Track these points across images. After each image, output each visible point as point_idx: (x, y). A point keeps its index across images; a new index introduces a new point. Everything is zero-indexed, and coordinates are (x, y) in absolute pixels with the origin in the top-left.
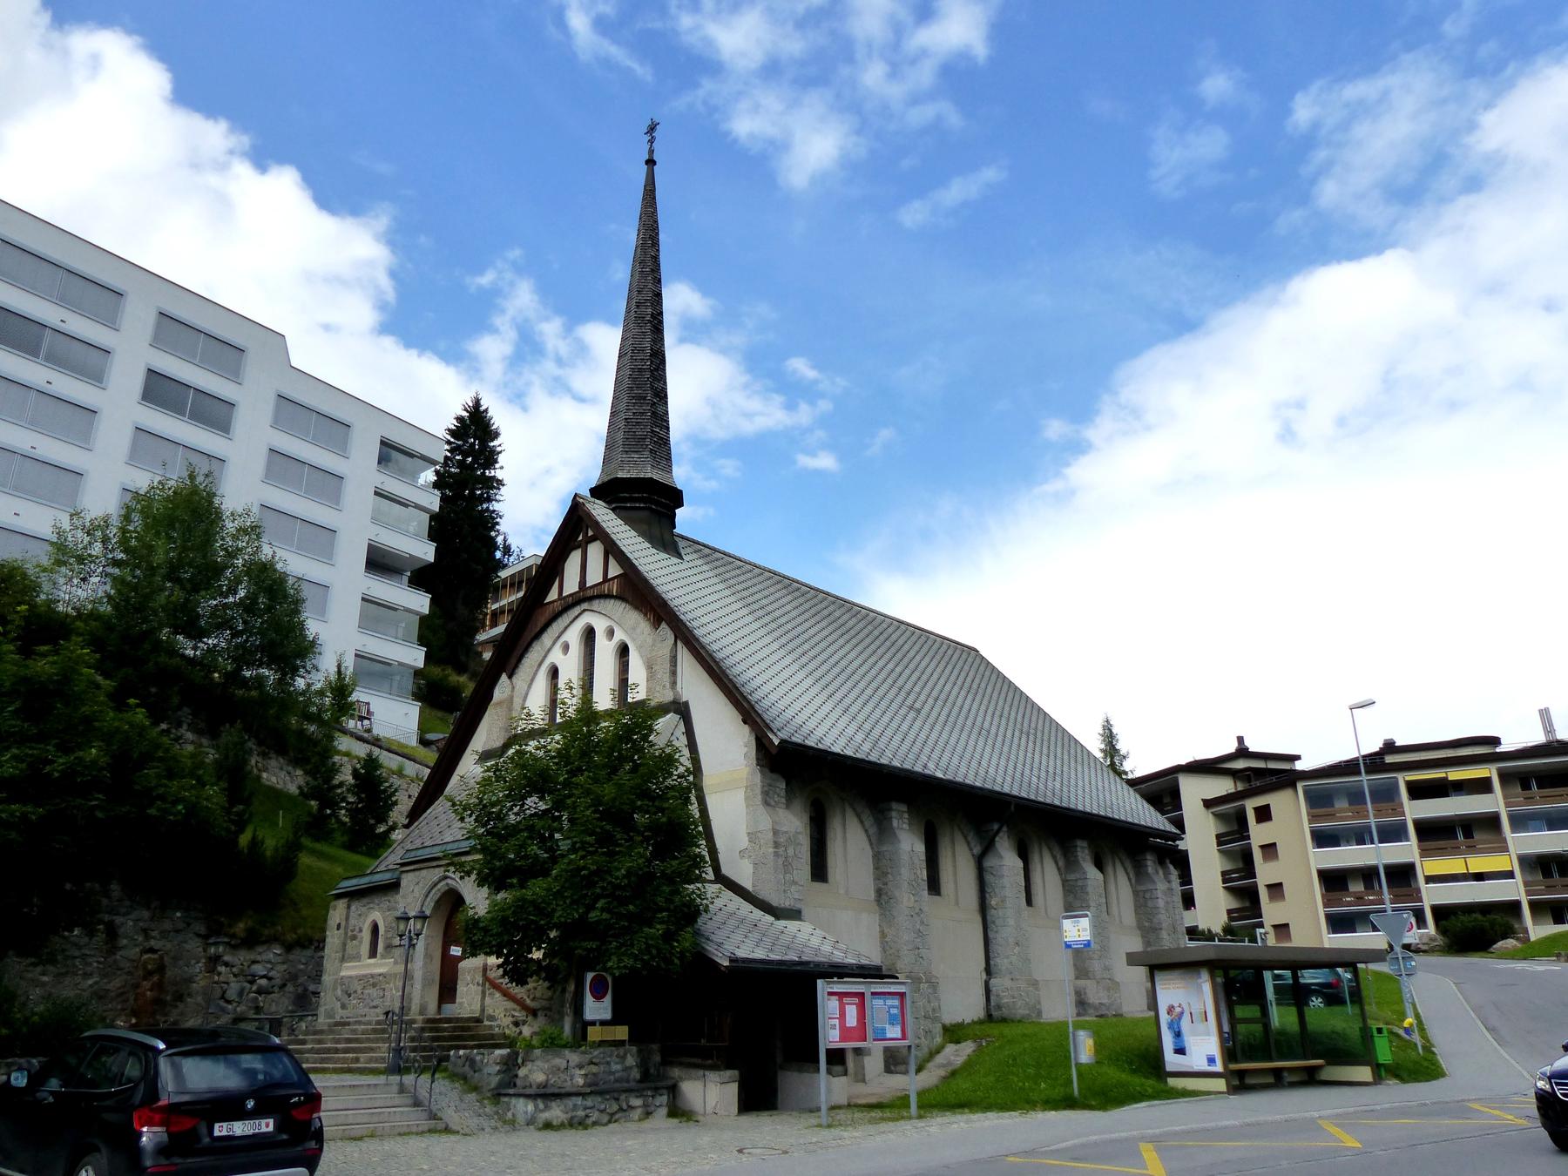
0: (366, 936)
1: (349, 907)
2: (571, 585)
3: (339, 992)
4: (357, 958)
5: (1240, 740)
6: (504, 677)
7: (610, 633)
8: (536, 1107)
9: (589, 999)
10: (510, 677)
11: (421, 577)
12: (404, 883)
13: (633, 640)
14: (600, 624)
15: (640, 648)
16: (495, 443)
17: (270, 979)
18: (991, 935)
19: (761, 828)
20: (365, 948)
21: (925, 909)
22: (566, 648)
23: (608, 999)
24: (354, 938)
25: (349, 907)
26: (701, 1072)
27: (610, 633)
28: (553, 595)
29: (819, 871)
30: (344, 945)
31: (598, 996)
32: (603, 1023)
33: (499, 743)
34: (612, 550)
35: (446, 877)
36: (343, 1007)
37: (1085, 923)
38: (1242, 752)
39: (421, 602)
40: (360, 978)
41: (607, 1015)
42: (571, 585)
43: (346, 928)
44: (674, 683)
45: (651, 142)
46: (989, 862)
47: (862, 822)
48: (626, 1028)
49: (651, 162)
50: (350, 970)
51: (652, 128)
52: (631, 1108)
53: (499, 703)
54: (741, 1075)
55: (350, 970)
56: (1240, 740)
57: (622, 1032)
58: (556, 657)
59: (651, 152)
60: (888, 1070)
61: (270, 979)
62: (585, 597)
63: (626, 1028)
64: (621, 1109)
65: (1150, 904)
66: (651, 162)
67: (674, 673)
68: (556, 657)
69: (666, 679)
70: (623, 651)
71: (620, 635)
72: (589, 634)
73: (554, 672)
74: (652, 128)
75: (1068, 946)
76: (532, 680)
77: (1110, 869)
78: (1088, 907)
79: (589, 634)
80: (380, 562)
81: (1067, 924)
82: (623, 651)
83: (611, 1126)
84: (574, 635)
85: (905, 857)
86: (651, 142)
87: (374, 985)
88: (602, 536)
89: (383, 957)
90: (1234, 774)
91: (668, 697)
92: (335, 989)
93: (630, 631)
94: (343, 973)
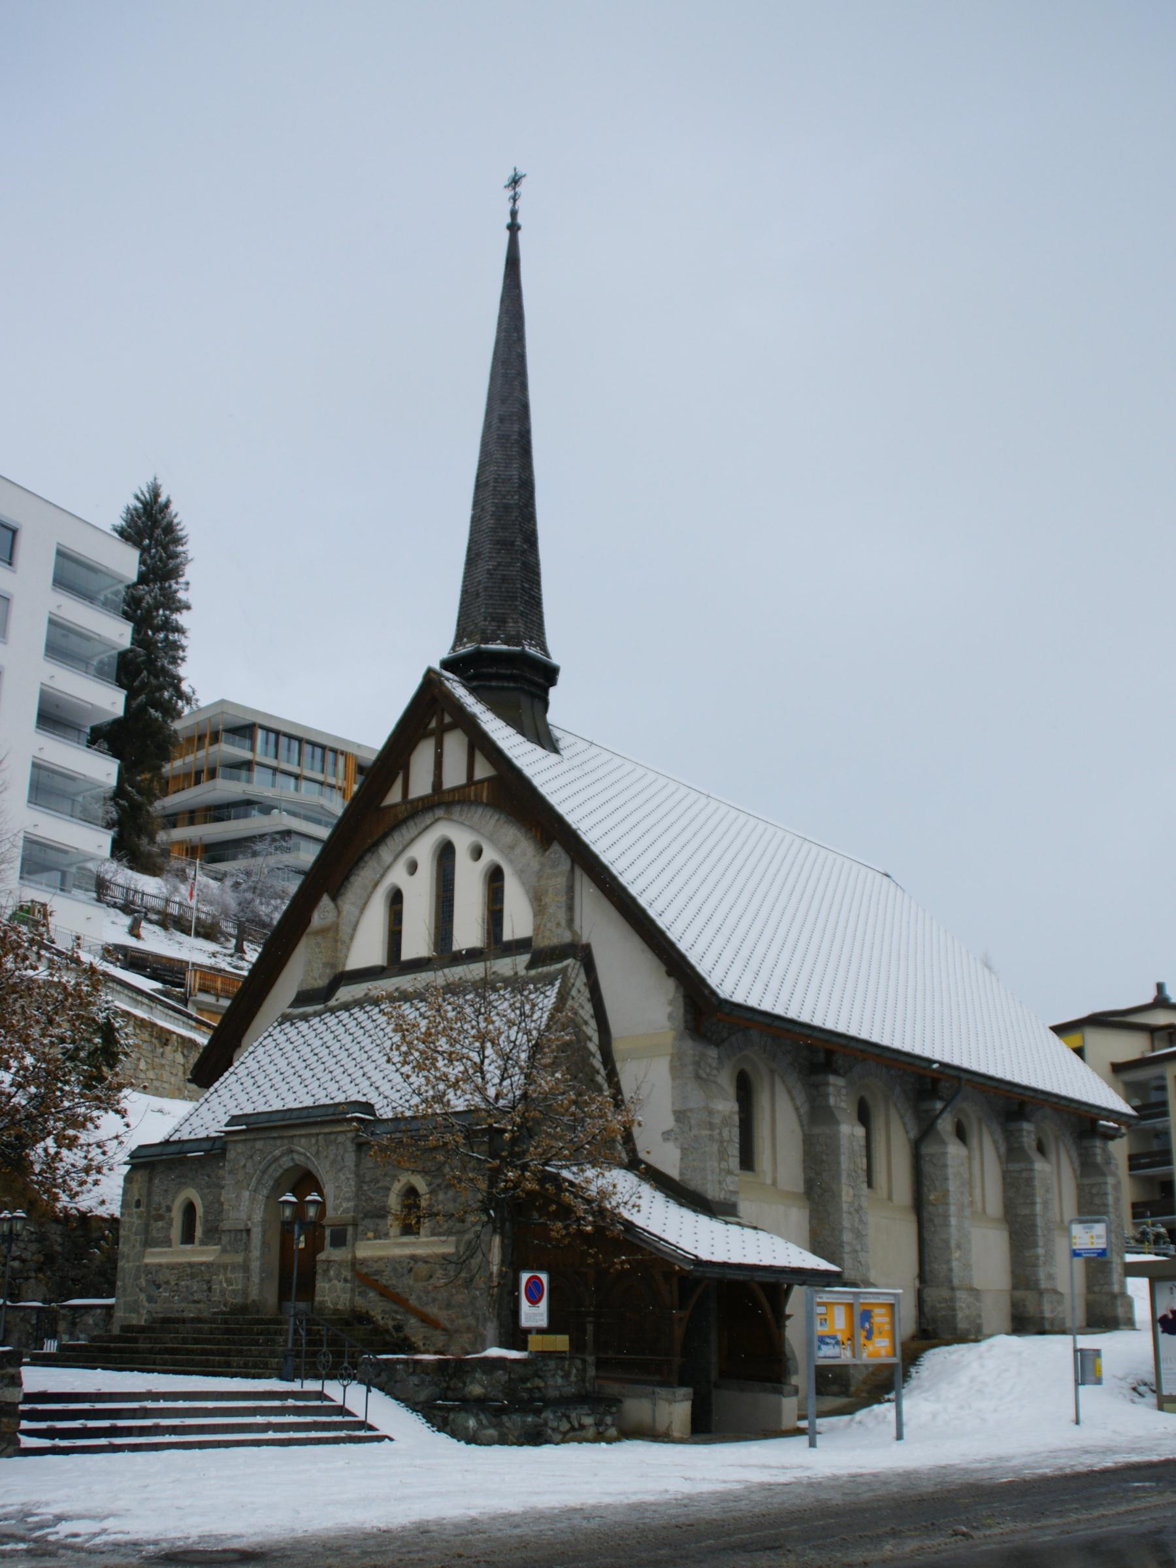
0: (177, 1215)
1: (150, 1181)
2: (421, 784)
3: (143, 1282)
4: (167, 1242)
5: (1160, 987)
6: (326, 900)
7: (477, 853)
8: (479, 1422)
9: (525, 1303)
10: (334, 898)
11: (106, 737)
12: (231, 1155)
13: (511, 861)
14: (462, 840)
15: (520, 873)
16: (180, 549)
17: (23, 1261)
18: (926, 1236)
19: (692, 1105)
20: (176, 1232)
21: (865, 1204)
22: (413, 868)
23: (544, 1304)
24: (160, 1218)
25: (150, 1181)
26: (649, 1389)
27: (477, 853)
28: (394, 796)
29: (747, 1161)
30: (147, 1225)
31: (534, 1301)
32: (540, 1331)
33: (321, 983)
34: (480, 743)
35: (291, 1151)
36: (150, 1299)
37: (1100, 1229)
38: (1161, 1002)
39: (103, 770)
40: (172, 1267)
41: (543, 1322)
42: (421, 784)
43: (148, 1205)
44: (570, 921)
45: (514, 199)
46: (927, 1149)
47: (793, 1099)
48: (566, 1338)
49: (513, 228)
50: (155, 1257)
51: (515, 182)
52: (582, 1427)
53: (323, 932)
54: (695, 1394)
55: (155, 1257)
56: (1160, 987)
57: (561, 1342)
58: (398, 876)
59: (514, 214)
60: (820, 1392)
61: (23, 1261)
62: (441, 801)
63: (566, 1338)
64: (573, 1429)
65: (1097, 1201)
66: (513, 228)
67: (570, 908)
68: (398, 876)
69: (562, 916)
70: (495, 877)
71: (490, 855)
72: (446, 852)
73: (396, 898)
74: (515, 182)
75: (1075, 1254)
76: (366, 904)
77: (974, 1142)
78: (1106, 1213)
79: (446, 852)
80: (53, 717)
81: (1077, 1230)
82: (495, 877)
83: (562, 1446)
84: (424, 850)
85: (844, 1143)
86: (514, 199)
87: (193, 1276)
88: (470, 726)
89: (203, 1243)
90: (1152, 1030)
91: (567, 937)
92: (137, 1278)
93: (508, 850)
94: (147, 1260)
